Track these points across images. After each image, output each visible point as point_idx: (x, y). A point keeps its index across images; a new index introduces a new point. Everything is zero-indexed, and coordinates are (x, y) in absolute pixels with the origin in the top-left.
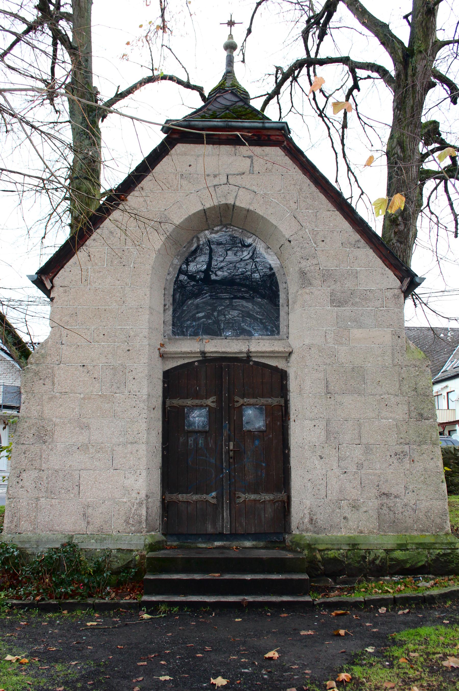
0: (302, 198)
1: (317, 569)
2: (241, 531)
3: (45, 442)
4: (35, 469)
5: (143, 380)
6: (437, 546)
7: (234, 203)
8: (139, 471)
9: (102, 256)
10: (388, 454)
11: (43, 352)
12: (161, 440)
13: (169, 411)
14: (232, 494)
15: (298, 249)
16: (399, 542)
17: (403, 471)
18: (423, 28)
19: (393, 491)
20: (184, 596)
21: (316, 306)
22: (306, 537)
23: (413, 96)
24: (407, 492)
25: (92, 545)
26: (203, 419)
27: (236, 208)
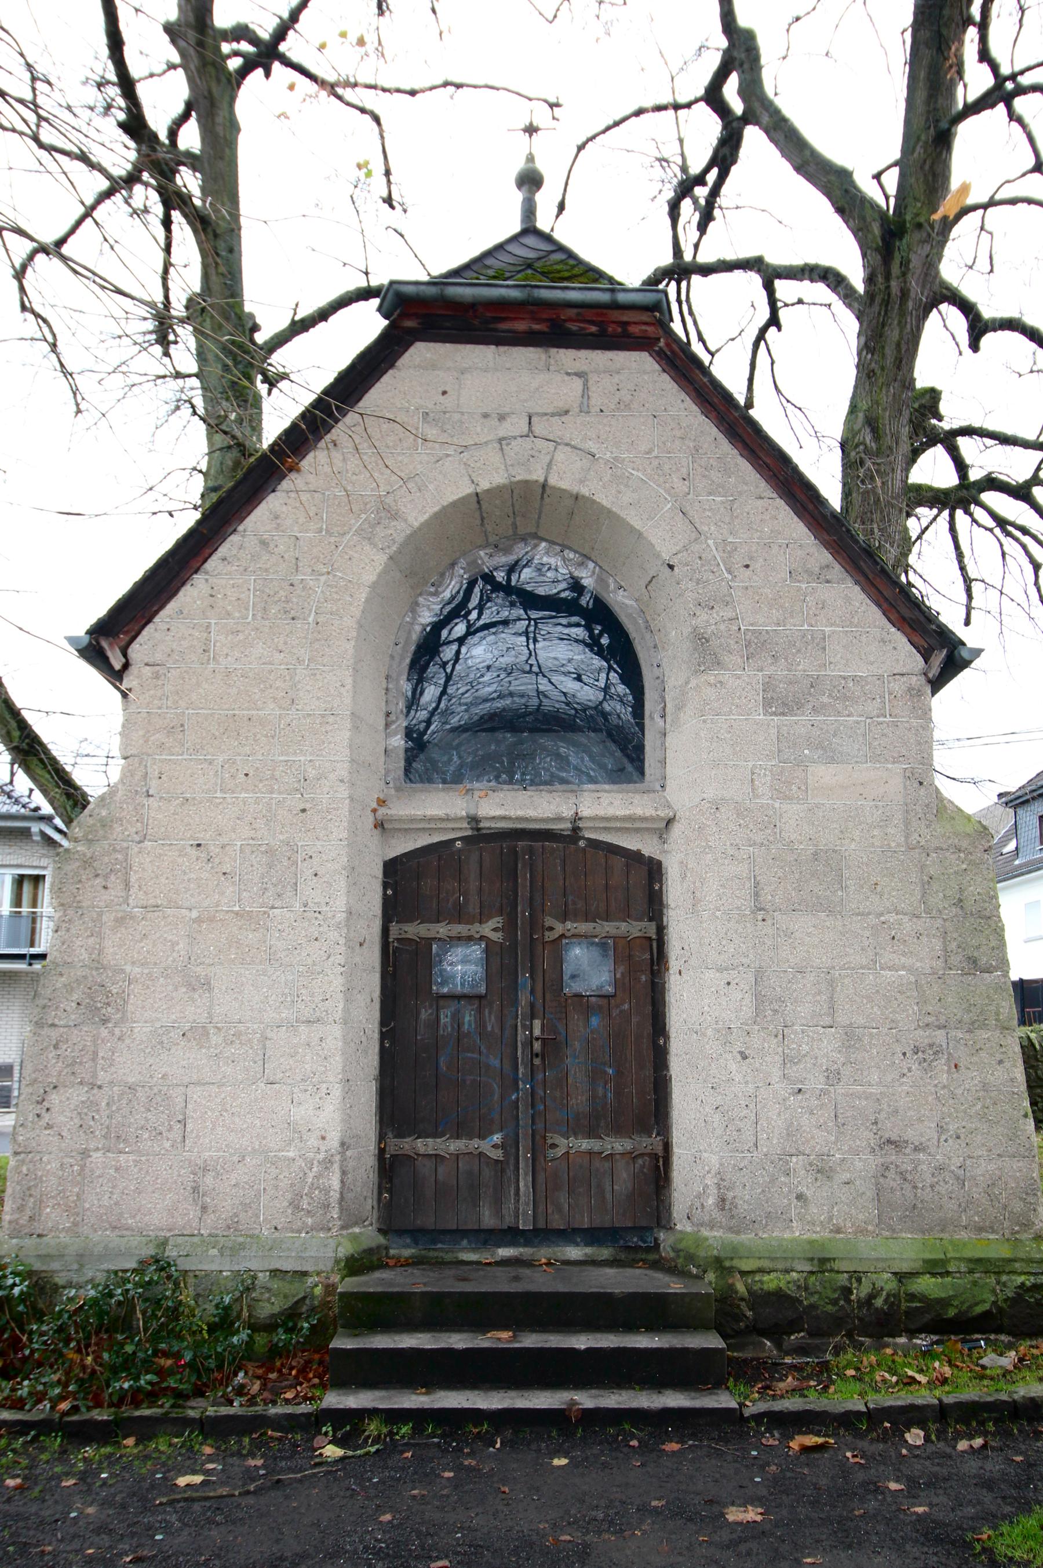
0: (700, 470)
1: (740, 1317)
2: (557, 1222)
3: (105, 1021)
4: (81, 1083)
5: (336, 878)
6: (1017, 1265)
7: (546, 480)
8: (325, 1085)
9: (242, 596)
10: (899, 1050)
11: (104, 813)
12: (377, 1015)
13: (395, 950)
14: (538, 1137)
15: (691, 585)
16: (928, 1256)
17: (933, 1090)
18: (925, 175)
19: (910, 1134)
20: (427, 1393)
21: (731, 712)
22: (710, 1241)
23: (900, 322)
24: (943, 1137)
25: (213, 1263)
26: (473, 967)
27: (548, 491)
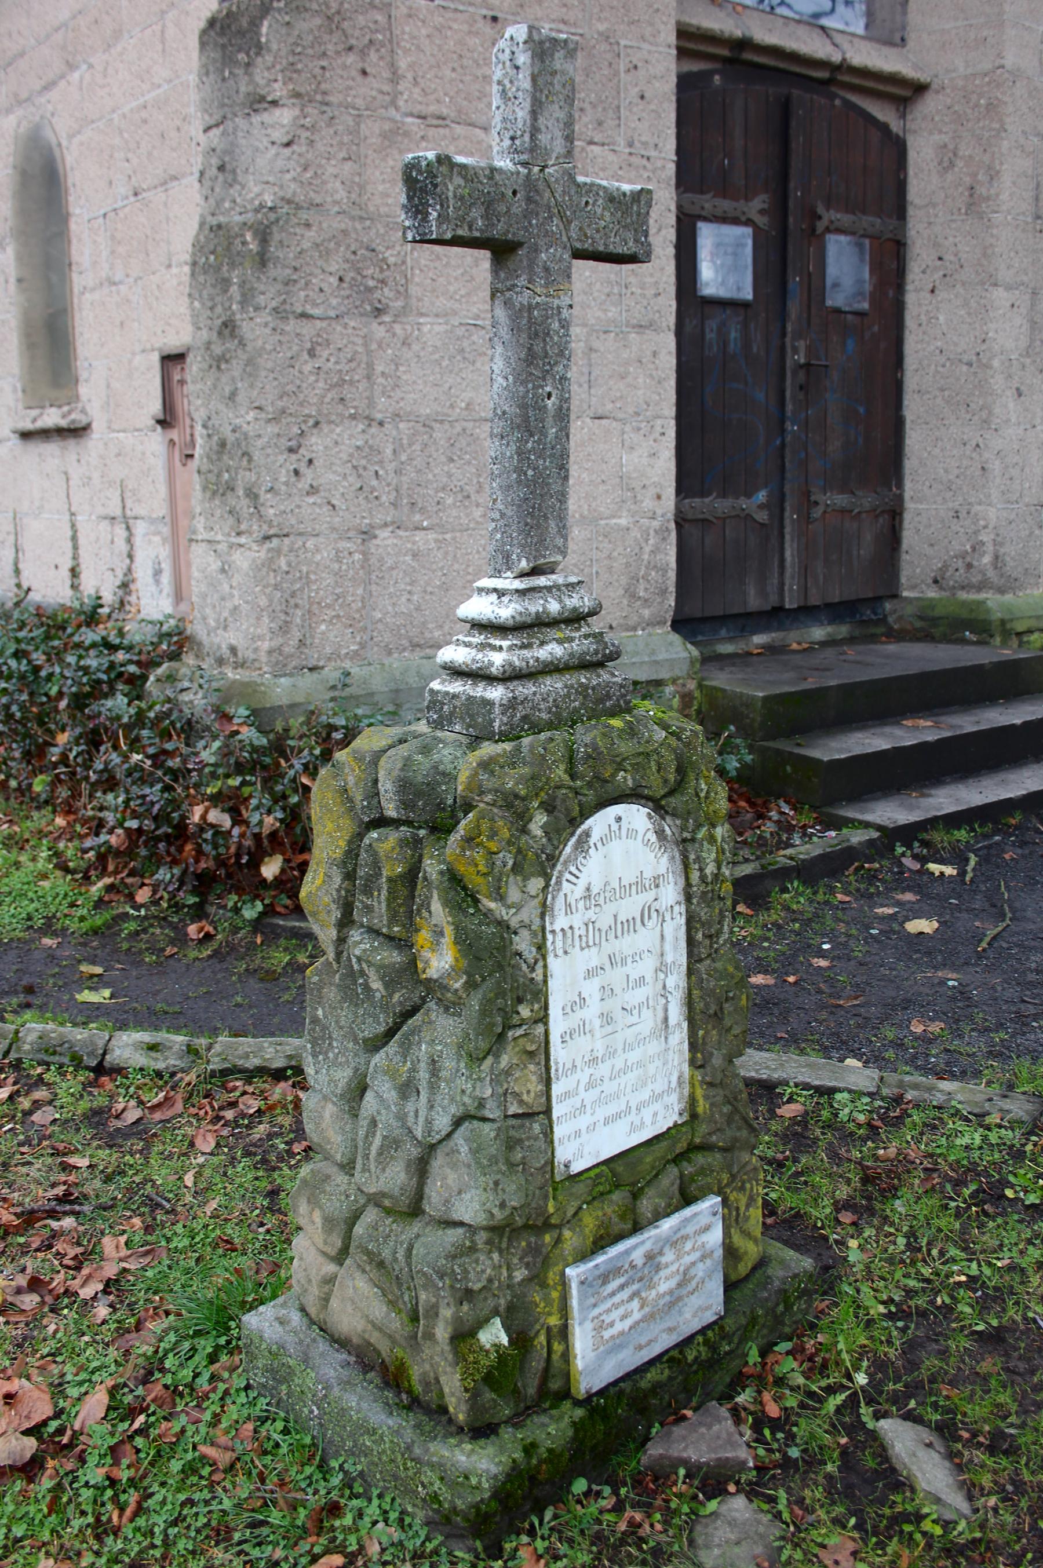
3: (378, 312)
8: (659, 422)
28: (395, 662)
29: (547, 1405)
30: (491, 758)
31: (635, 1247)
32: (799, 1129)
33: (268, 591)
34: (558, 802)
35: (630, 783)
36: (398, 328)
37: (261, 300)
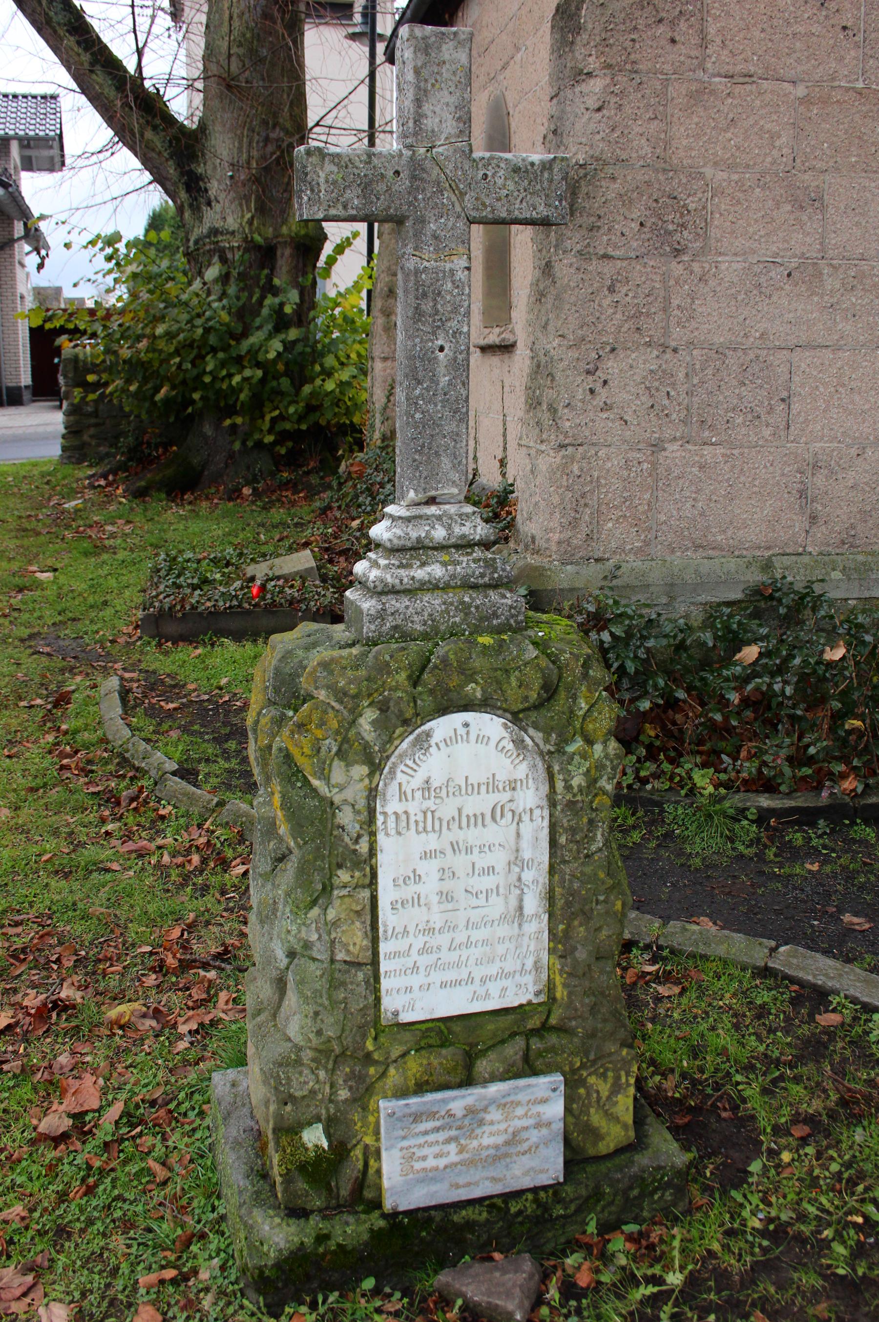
3: (677, 252)
28: (677, 559)
29: (361, 1208)
30: (332, 660)
31: (454, 1099)
32: (825, 1038)
33: (560, 491)
34: (391, 704)
35: (479, 694)
36: (696, 266)
37: (568, 244)
